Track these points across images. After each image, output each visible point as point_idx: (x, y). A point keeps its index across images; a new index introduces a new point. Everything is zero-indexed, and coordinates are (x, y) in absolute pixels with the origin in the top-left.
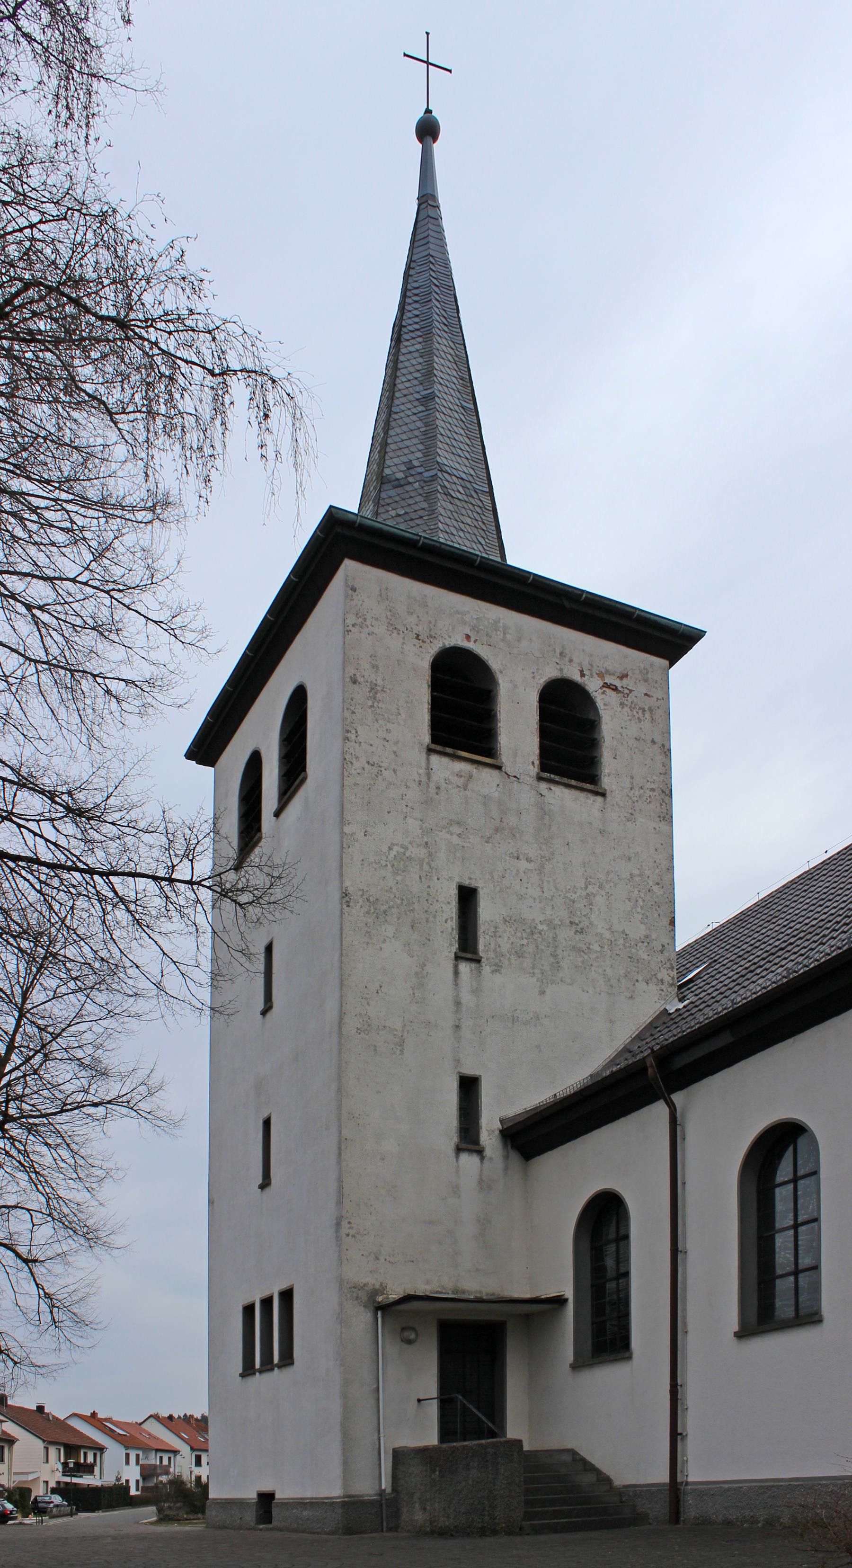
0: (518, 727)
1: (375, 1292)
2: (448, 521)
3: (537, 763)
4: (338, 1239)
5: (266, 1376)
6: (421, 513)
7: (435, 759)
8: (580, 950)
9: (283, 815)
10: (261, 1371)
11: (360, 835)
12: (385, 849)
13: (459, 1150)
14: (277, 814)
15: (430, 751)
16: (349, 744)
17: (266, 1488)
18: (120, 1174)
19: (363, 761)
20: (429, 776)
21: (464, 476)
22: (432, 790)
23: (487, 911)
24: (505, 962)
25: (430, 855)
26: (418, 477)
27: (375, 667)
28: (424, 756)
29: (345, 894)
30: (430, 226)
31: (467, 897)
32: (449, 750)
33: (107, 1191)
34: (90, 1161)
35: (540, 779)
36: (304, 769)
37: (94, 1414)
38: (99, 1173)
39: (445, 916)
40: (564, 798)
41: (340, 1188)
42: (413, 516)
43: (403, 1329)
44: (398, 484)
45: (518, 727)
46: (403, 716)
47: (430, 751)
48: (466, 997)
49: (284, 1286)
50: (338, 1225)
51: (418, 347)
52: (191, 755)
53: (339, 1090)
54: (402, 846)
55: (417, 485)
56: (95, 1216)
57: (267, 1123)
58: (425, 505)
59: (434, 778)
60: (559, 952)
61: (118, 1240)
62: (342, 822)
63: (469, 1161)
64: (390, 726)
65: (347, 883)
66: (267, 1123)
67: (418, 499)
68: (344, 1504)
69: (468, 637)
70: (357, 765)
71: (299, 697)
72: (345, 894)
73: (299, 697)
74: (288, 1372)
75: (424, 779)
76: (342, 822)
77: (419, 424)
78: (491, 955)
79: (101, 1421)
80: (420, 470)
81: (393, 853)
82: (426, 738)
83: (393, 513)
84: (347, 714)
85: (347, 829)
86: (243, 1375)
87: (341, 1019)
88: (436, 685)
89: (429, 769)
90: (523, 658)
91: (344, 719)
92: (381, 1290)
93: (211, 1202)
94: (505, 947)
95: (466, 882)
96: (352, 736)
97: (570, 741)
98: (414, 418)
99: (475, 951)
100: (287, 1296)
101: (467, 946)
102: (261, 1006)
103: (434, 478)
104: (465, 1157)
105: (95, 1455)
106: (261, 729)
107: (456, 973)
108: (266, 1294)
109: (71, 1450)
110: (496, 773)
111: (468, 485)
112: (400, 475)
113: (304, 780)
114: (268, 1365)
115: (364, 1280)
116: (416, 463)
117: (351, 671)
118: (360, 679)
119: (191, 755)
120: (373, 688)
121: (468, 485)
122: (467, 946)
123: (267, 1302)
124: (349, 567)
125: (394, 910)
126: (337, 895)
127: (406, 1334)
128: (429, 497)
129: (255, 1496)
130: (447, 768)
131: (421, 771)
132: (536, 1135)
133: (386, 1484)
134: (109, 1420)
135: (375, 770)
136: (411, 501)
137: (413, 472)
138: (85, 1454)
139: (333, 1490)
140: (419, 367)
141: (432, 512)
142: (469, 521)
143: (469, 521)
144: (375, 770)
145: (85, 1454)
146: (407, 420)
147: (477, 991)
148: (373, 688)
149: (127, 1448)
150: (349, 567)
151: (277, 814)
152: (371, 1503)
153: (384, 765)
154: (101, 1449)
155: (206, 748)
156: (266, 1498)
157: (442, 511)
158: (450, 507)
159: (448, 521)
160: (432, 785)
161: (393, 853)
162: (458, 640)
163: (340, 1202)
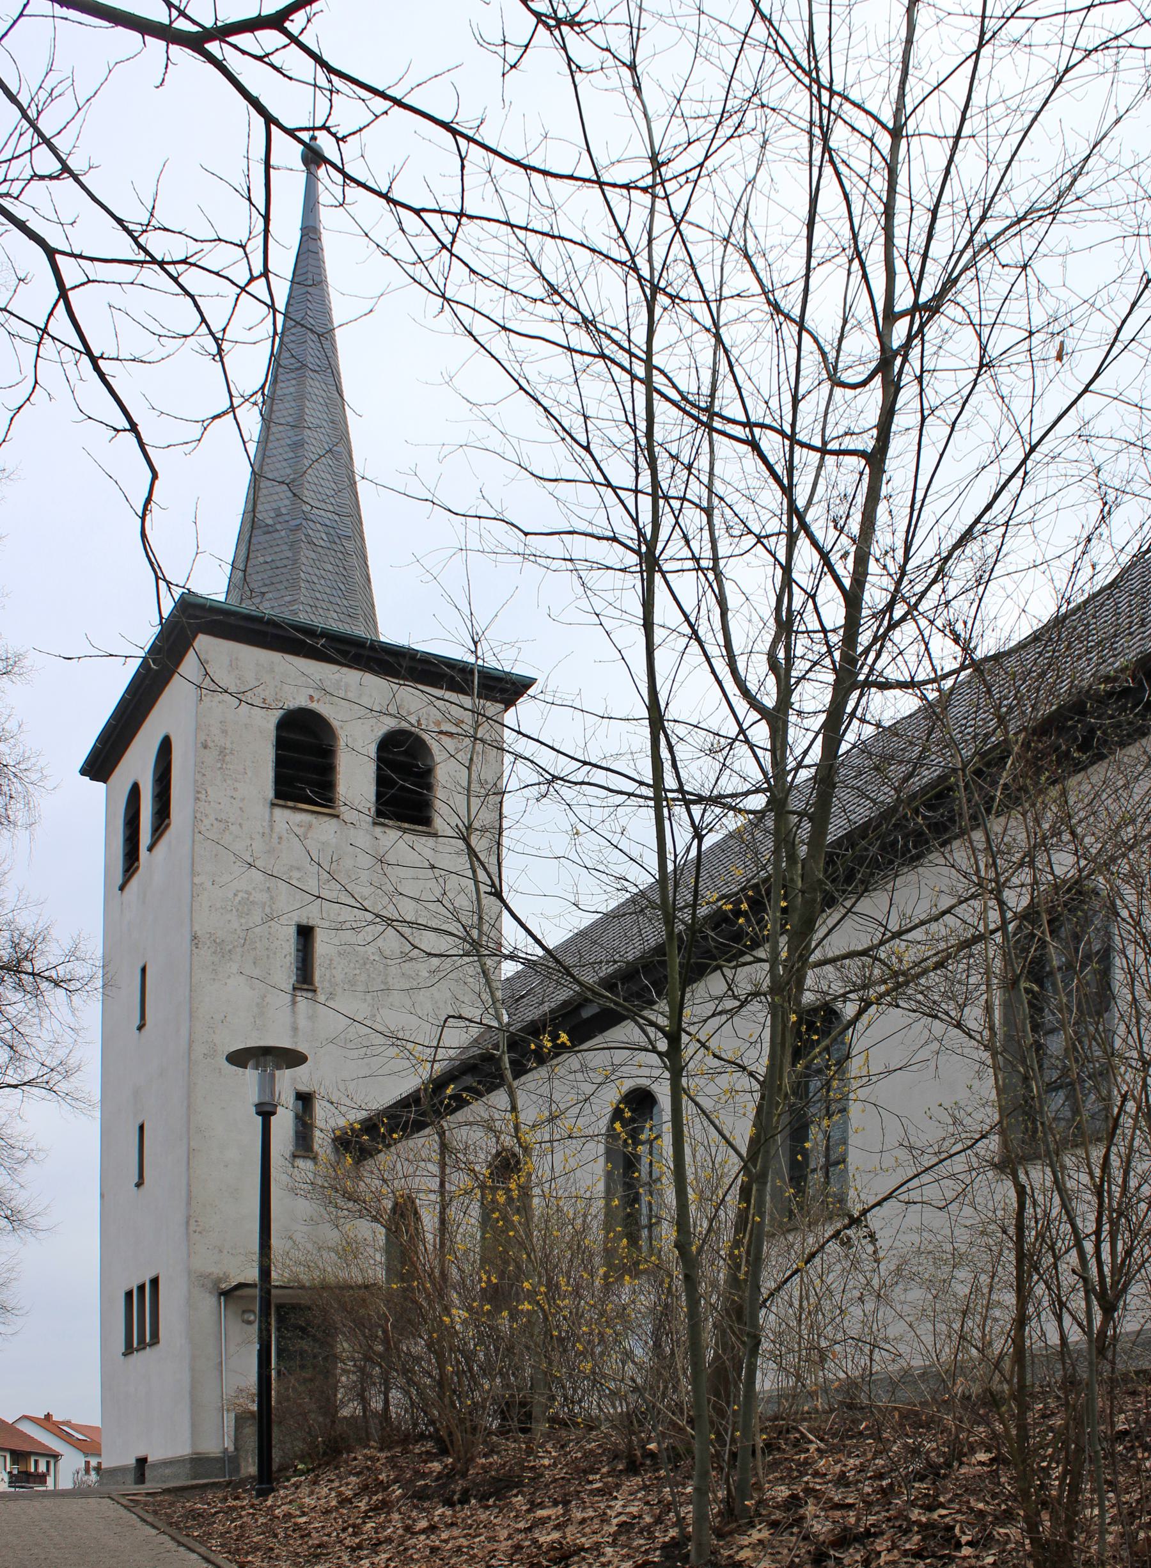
0: (356, 777)
1: (219, 1280)
2: (310, 570)
3: (373, 809)
4: (188, 1234)
5: (142, 1353)
6: (285, 562)
7: (278, 812)
8: (410, 977)
9: (156, 850)
10: (138, 1350)
11: (208, 884)
12: (231, 896)
13: (294, 1156)
14: (150, 849)
15: (273, 805)
16: (200, 804)
17: (141, 1454)
18: (42, 1155)
19: (212, 818)
20: (272, 828)
21: (328, 523)
22: (275, 840)
23: (322, 946)
24: (339, 990)
25: (272, 898)
26: (285, 525)
27: (225, 732)
28: (268, 810)
29: (195, 938)
30: (311, 261)
31: (305, 933)
32: (290, 804)
33: (29, 1172)
34: (11, 1142)
35: (375, 824)
36: (168, 816)
37: (48, 1417)
38: (20, 1154)
39: (285, 952)
40: (395, 840)
41: (189, 1192)
42: (279, 564)
43: (244, 1312)
44: (269, 530)
45: (356, 777)
46: (249, 774)
47: (273, 805)
48: (303, 1023)
49: (152, 1275)
50: (188, 1223)
51: (292, 390)
52: (84, 772)
53: (189, 1107)
54: (247, 892)
55: (283, 533)
56: (19, 1199)
57: (141, 1128)
58: (289, 554)
59: (277, 829)
60: (390, 980)
61: (42, 1222)
62: (193, 873)
63: (304, 1164)
64: (237, 785)
65: (196, 928)
66: (141, 1128)
67: (285, 547)
68: (192, 1460)
69: (311, 697)
70: (206, 822)
71: (166, 746)
72: (195, 938)
73: (166, 746)
74: (156, 1348)
75: (267, 831)
76: (193, 873)
77: (288, 471)
78: (326, 984)
79: (56, 1424)
80: (287, 518)
81: (238, 899)
82: (270, 793)
83: (261, 559)
84: (198, 777)
85: (197, 880)
86: (125, 1355)
87: (190, 1046)
88: (281, 744)
89: (272, 821)
90: (360, 714)
91: (196, 781)
92: (226, 1277)
93: (102, 1196)
94: (339, 977)
95: (304, 922)
96: (203, 796)
97: (404, 788)
98: (284, 464)
99: (311, 983)
100: (155, 1282)
101: (305, 976)
102: (137, 1022)
103: (298, 527)
104: (300, 1163)
105: (48, 1463)
106: (138, 763)
107: (294, 1003)
108: (140, 1282)
109: (18, 1456)
110: (334, 820)
111: (332, 531)
112: (270, 522)
113: (168, 826)
114: (143, 1346)
115: (209, 1270)
116: (284, 511)
117: (202, 737)
118: (210, 744)
119: (84, 772)
120: (222, 752)
121: (332, 531)
122: (305, 976)
123: (141, 1288)
124: (203, 641)
125: (239, 950)
126: (188, 937)
127: (246, 1316)
128: (293, 545)
129: (133, 1461)
130: (289, 819)
131: (265, 824)
132: (365, 1140)
133: (229, 1444)
134: (68, 1423)
135: (223, 826)
136: (277, 549)
137: (280, 519)
138: (36, 1462)
139: (182, 1449)
140: (291, 411)
141: (295, 561)
142: (330, 567)
143: (330, 567)
144: (223, 826)
145: (36, 1462)
146: (278, 465)
147: (312, 1018)
148: (222, 752)
149: (86, 1454)
150: (203, 641)
151: (150, 849)
152: (216, 1459)
153: (232, 820)
154: (56, 1456)
155: (99, 766)
156: (142, 1462)
157: (304, 560)
158: (313, 555)
159: (310, 570)
160: (275, 836)
161: (238, 899)
162: (301, 701)
163: (189, 1203)
